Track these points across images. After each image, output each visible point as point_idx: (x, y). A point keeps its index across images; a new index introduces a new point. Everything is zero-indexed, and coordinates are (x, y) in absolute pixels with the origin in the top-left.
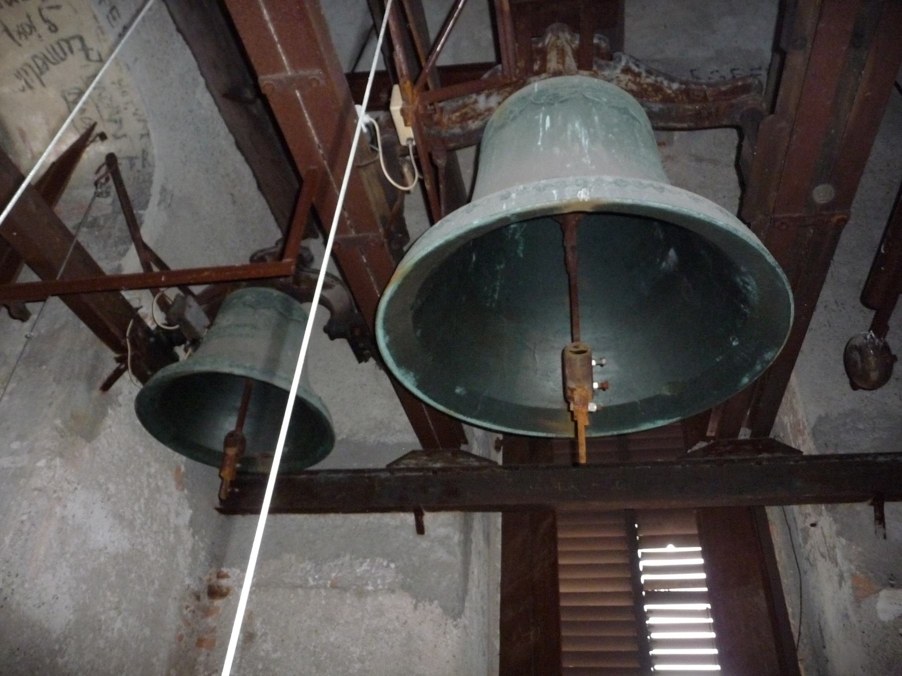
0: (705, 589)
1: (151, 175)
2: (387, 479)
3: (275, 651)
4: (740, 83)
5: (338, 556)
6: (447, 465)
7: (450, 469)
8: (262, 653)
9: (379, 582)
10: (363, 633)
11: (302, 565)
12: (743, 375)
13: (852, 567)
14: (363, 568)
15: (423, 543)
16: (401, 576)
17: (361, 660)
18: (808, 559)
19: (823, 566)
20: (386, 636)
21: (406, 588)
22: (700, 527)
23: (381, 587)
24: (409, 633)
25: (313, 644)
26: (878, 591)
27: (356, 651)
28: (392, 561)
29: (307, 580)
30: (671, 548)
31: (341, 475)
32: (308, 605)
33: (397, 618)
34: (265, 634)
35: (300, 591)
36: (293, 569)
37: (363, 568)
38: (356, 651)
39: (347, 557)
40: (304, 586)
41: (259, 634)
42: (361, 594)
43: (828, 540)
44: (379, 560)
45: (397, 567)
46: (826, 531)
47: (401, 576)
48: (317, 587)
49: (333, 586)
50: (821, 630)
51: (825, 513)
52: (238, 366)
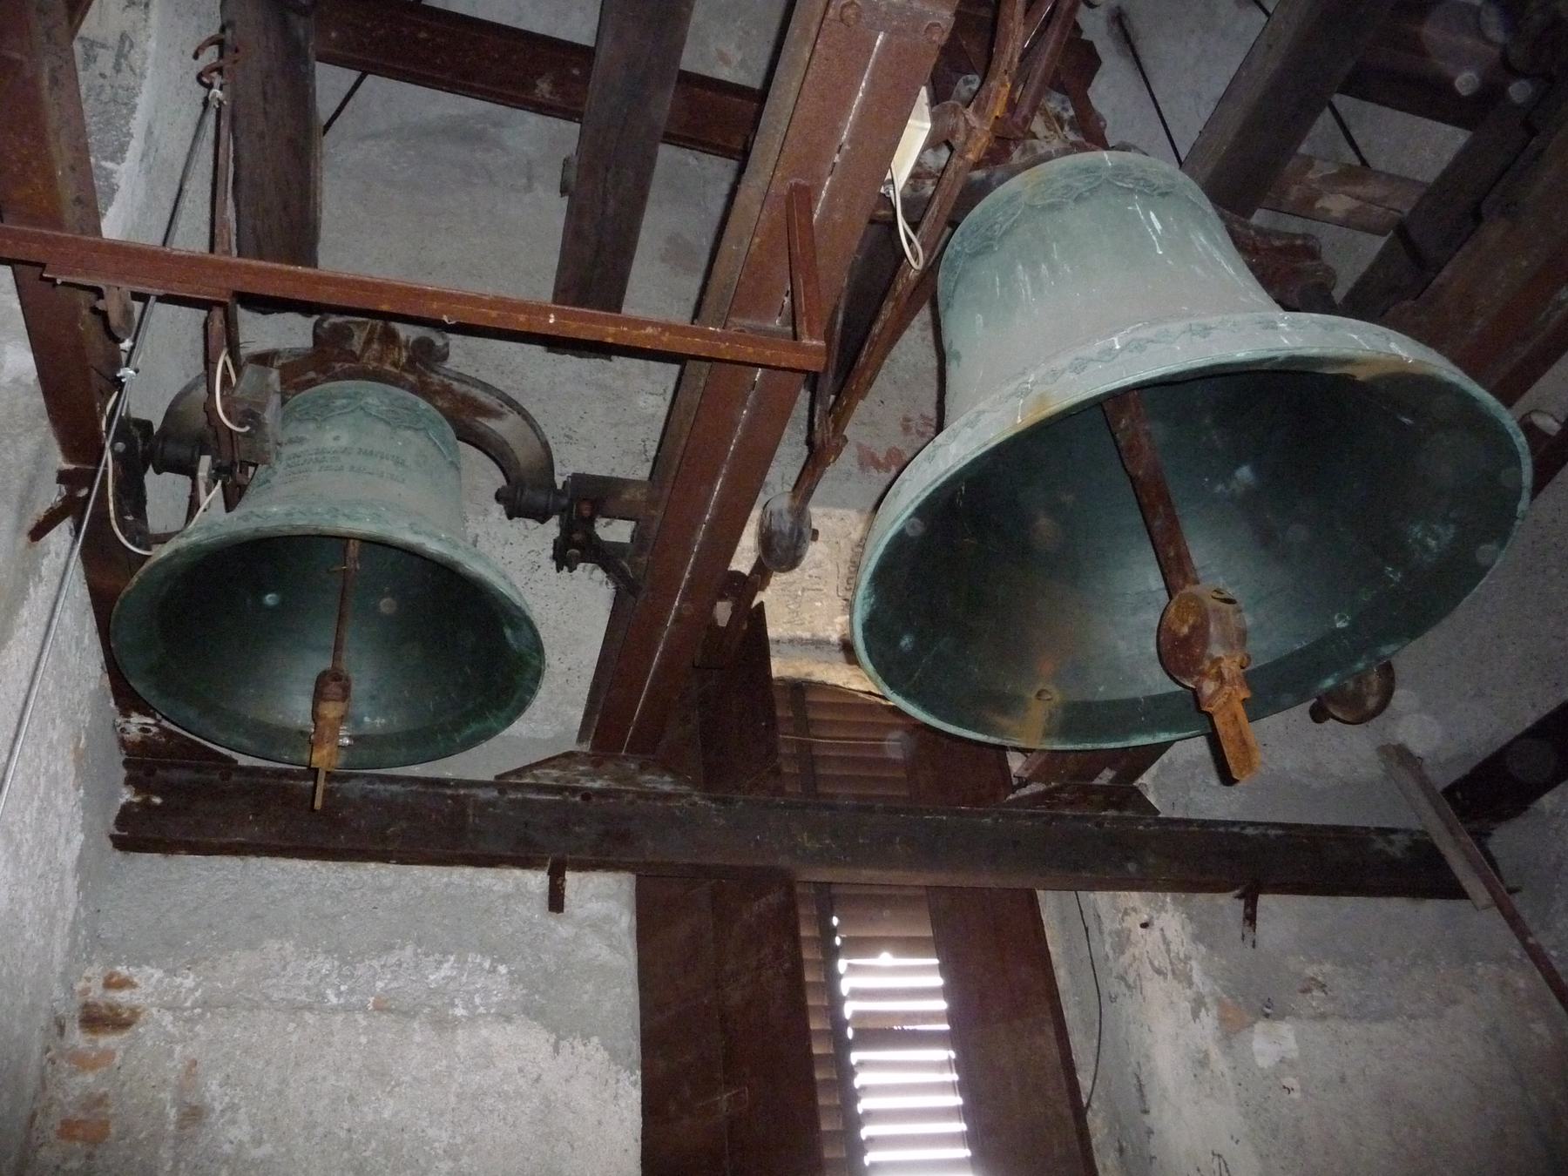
0: (946, 1027)
1: (132, 92)
2: (491, 803)
3: (258, 1142)
4: (1299, 242)
5: (389, 948)
6: (614, 786)
7: (617, 794)
8: (227, 1148)
9: (477, 1000)
10: (453, 1099)
11: (310, 965)
12: (1327, 676)
13: (1218, 989)
14: (442, 973)
15: (562, 928)
16: (520, 990)
17: (452, 1153)
18: (1122, 978)
19: (1155, 988)
20: (501, 1106)
21: (533, 1012)
22: (935, 924)
23: (482, 1010)
24: (545, 1098)
25: (346, 1126)
26: (1251, 1025)
27: (441, 1137)
28: (502, 961)
29: (324, 996)
30: (886, 959)
31: (395, 788)
32: (329, 1044)
33: (521, 1070)
34: (233, 1107)
35: (309, 1017)
36: (290, 971)
37: (442, 973)
38: (441, 1137)
39: (409, 951)
40: (317, 1004)
41: (218, 1107)
42: (443, 1023)
43: (1173, 947)
44: (474, 958)
45: (510, 972)
46: (1169, 935)
47: (520, 990)
48: (347, 1009)
49: (380, 1008)
50: (1140, 1088)
51: (1170, 907)
52: (430, 535)
